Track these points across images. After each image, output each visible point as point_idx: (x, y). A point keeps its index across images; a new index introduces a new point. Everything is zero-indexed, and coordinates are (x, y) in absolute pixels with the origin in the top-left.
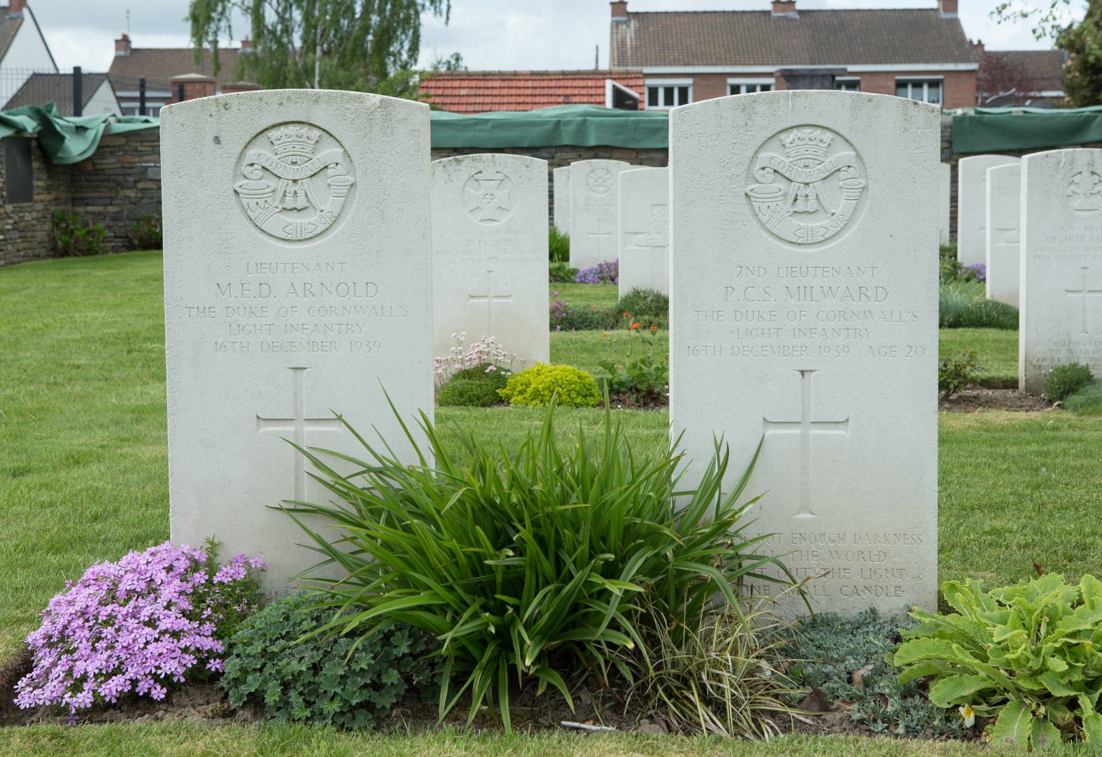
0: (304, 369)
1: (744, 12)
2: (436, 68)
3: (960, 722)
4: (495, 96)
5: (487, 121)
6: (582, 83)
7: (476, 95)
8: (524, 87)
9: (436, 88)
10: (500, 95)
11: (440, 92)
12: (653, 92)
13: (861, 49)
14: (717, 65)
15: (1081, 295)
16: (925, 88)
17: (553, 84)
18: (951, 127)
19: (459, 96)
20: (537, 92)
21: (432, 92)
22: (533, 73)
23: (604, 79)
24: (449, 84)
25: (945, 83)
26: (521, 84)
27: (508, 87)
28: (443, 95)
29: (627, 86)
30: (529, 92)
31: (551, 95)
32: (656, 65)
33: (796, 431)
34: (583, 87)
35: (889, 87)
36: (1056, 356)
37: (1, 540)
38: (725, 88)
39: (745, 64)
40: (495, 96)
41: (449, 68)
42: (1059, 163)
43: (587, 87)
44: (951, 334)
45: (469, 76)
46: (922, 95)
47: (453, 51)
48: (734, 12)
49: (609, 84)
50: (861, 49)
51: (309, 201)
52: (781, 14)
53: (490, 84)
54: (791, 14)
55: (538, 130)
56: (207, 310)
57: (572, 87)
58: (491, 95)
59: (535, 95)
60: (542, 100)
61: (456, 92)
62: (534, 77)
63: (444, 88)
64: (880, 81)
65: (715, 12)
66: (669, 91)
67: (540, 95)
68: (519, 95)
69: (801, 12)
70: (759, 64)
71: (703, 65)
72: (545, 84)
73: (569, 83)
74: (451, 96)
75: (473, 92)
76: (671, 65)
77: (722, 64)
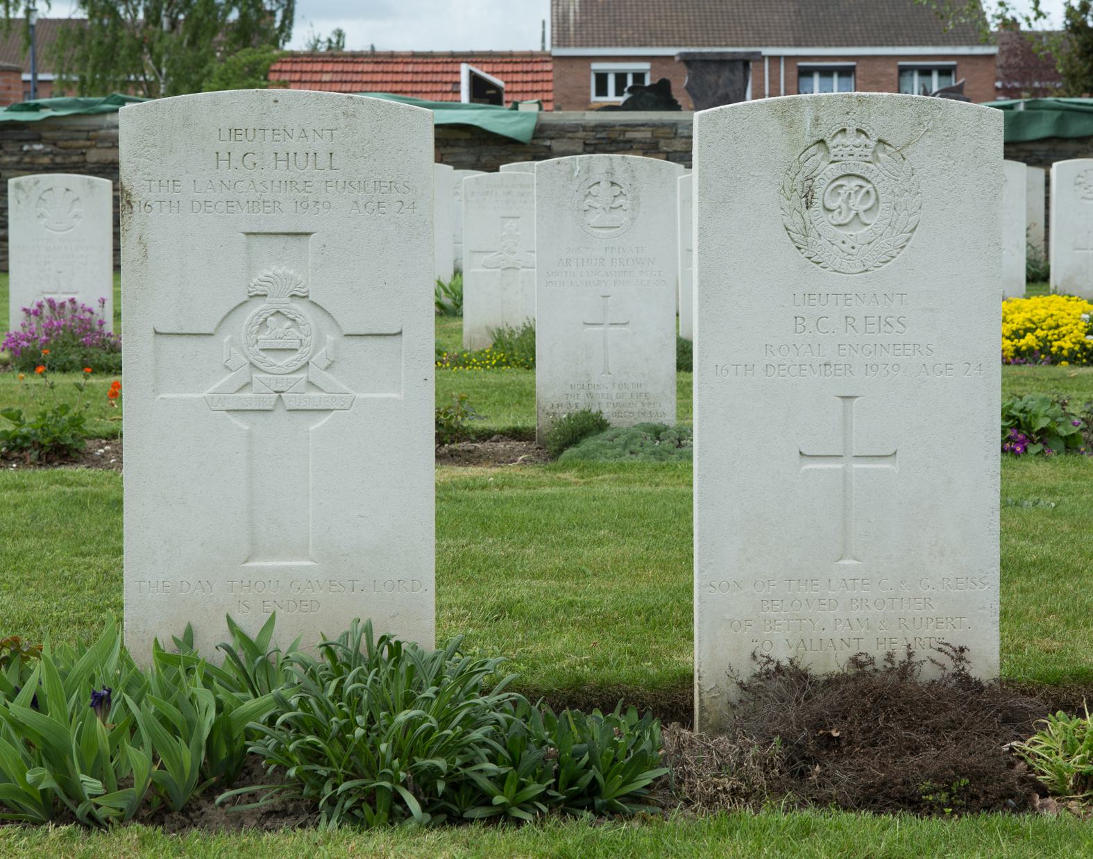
2: (315, 48)
3: (116, 822)
8: (402, 72)
9: (291, 72)
10: (372, 82)
12: (602, 78)
13: (858, 28)
15: (601, 328)
16: (935, 76)
17: (439, 68)
20: (419, 78)
22: (414, 55)
24: (308, 67)
25: (958, 70)
26: (399, 68)
27: (383, 72)
29: (492, 73)
30: (409, 78)
31: (436, 82)
32: (605, 46)
36: (574, 401)
37: (2, 607)
40: (366, 82)
42: (572, 171)
44: (1015, 370)
45: (355, 57)
46: (832, 85)
50: (858, 28)
53: (360, 68)
58: (361, 82)
59: (416, 82)
60: (424, 88)
62: (415, 60)
63: (302, 72)
66: (621, 78)
67: (422, 82)
68: (396, 82)
71: (663, 45)
72: (429, 68)
76: (623, 46)
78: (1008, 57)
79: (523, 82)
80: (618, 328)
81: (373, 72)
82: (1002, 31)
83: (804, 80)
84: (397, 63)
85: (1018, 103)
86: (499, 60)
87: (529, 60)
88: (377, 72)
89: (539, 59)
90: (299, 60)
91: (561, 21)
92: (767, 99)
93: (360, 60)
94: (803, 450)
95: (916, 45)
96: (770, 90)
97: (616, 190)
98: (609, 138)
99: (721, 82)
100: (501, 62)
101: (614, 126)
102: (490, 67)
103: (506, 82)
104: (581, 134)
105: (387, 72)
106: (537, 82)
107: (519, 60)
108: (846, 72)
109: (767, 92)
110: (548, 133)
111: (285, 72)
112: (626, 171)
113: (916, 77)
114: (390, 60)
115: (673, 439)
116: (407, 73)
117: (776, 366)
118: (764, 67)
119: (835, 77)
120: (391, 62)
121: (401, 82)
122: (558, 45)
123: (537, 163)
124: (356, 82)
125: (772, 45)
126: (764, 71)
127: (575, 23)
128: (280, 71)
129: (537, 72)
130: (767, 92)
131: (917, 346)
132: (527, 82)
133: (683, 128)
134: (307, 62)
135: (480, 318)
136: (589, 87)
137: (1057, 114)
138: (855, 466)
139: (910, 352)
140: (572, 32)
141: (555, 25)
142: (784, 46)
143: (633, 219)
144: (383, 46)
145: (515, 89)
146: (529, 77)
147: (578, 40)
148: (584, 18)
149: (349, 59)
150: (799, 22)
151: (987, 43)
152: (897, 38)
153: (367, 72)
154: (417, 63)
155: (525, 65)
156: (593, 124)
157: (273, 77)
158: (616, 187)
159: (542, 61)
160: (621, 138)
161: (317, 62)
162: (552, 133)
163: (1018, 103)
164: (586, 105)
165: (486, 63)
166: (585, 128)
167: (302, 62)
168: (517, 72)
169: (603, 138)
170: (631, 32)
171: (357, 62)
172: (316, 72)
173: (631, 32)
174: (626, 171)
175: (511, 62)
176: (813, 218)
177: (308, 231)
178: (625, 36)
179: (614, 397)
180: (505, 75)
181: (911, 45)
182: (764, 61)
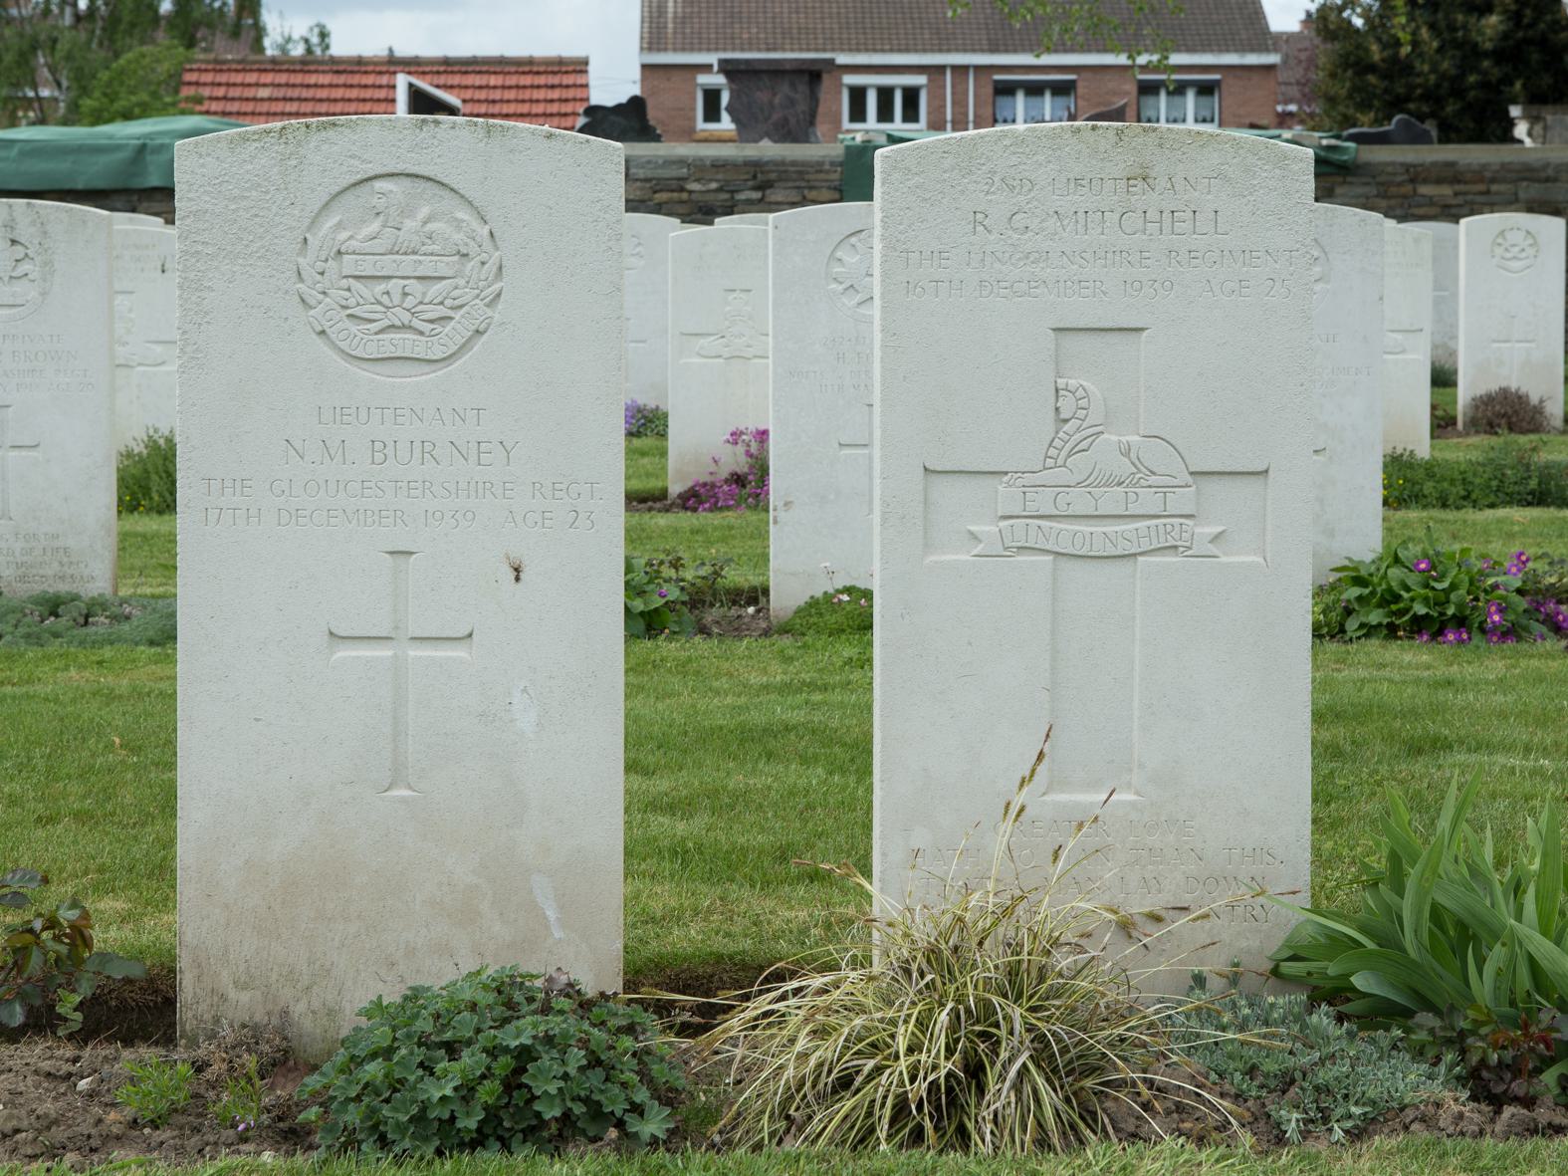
0: (412, 553)
4: (321, 100)
5: (13, 142)
6: (478, 80)
7: (285, 99)
8: (374, 86)
9: (213, 84)
10: (328, 100)
11: (220, 92)
12: (858, 95)
14: (858, 50)
16: (1190, 96)
18: (841, 164)
19: (254, 99)
21: (206, 92)
23: (395, 73)
24: (238, 78)
25: (1224, 86)
26: (369, 80)
28: (225, 98)
33: (384, 652)
34: (480, 87)
38: (840, 93)
39: (875, 51)
40: (321, 100)
41: (309, 51)
43: (487, 87)
47: (312, 22)
49: (402, 81)
53: (312, 79)
55: (104, 160)
56: (238, 484)
58: (313, 99)
61: (249, 93)
63: (228, 85)
66: (885, 95)
70: (900, 51)
74: (241, 99)
75: (280, 93)
78: (1307, 69)
79: (546, 101)
80: (24, 453)
81: (331, 86)
82: (1306, 32)
83: (1003, 101)
84: (366, 72)
86: (513, 69)
87: (556, 69)
88: (337, 86)
89: (570, 68)
90: (225, 67)
91: (655, 15)
92: (972, 132)
93: (312, 68)
94: (334, 631)
97: (19, 251)
99: (777, 100)
100: (517, 72)
103: (464, 101)
105: (352, 86)
106: (566, 100)
107: (542, 69)
108: (1062, 89)
111: (205, 84)
112: (33, 223)
113: (1020, 97)
114: (356, 68)
115: (75, 614)
116: (380, 87)
117: (293, 512)
118: (945, 81)
119: (1048, 96)
120: (358, 72)
121: (371, 100)
122: (650, 49)
123: (771, 216)
124: (306, 100)
125: (957, 50)
126: (944, 87)
127: (675, 17)
128: (197, 84)
129: (567, 86)
130: (1047, 117)
132: (552, 101)
133: (637, 167)
134: (237, 71)
135: (695, 446)
136: (693, 109)
138: (412, 653)
140: (670, 31)
141: (647, 19)
143: (44, 294)
145: (534, 111)
146: (556, 94)
147: (679, 41)
148: (688, 10)
149: (298, 67)
151: (1262, 48)
153: (322, 86)
155: (550, 77)
157: (186, 92)
158: (19, 247)
159: (574, 71)
161: (251, 70)
164: (689, 134)
165: (495, 73)
167: (229, 70)
168: (539, 87)
170: (755, 30)
171: (309, 72)
172: (249, 85)
173: (755, 30)
174: (33, 223)
175: (530, 72)
177: (1140, 325)
178: (745, 36)
179: (17, 554)
180: (463, 91)
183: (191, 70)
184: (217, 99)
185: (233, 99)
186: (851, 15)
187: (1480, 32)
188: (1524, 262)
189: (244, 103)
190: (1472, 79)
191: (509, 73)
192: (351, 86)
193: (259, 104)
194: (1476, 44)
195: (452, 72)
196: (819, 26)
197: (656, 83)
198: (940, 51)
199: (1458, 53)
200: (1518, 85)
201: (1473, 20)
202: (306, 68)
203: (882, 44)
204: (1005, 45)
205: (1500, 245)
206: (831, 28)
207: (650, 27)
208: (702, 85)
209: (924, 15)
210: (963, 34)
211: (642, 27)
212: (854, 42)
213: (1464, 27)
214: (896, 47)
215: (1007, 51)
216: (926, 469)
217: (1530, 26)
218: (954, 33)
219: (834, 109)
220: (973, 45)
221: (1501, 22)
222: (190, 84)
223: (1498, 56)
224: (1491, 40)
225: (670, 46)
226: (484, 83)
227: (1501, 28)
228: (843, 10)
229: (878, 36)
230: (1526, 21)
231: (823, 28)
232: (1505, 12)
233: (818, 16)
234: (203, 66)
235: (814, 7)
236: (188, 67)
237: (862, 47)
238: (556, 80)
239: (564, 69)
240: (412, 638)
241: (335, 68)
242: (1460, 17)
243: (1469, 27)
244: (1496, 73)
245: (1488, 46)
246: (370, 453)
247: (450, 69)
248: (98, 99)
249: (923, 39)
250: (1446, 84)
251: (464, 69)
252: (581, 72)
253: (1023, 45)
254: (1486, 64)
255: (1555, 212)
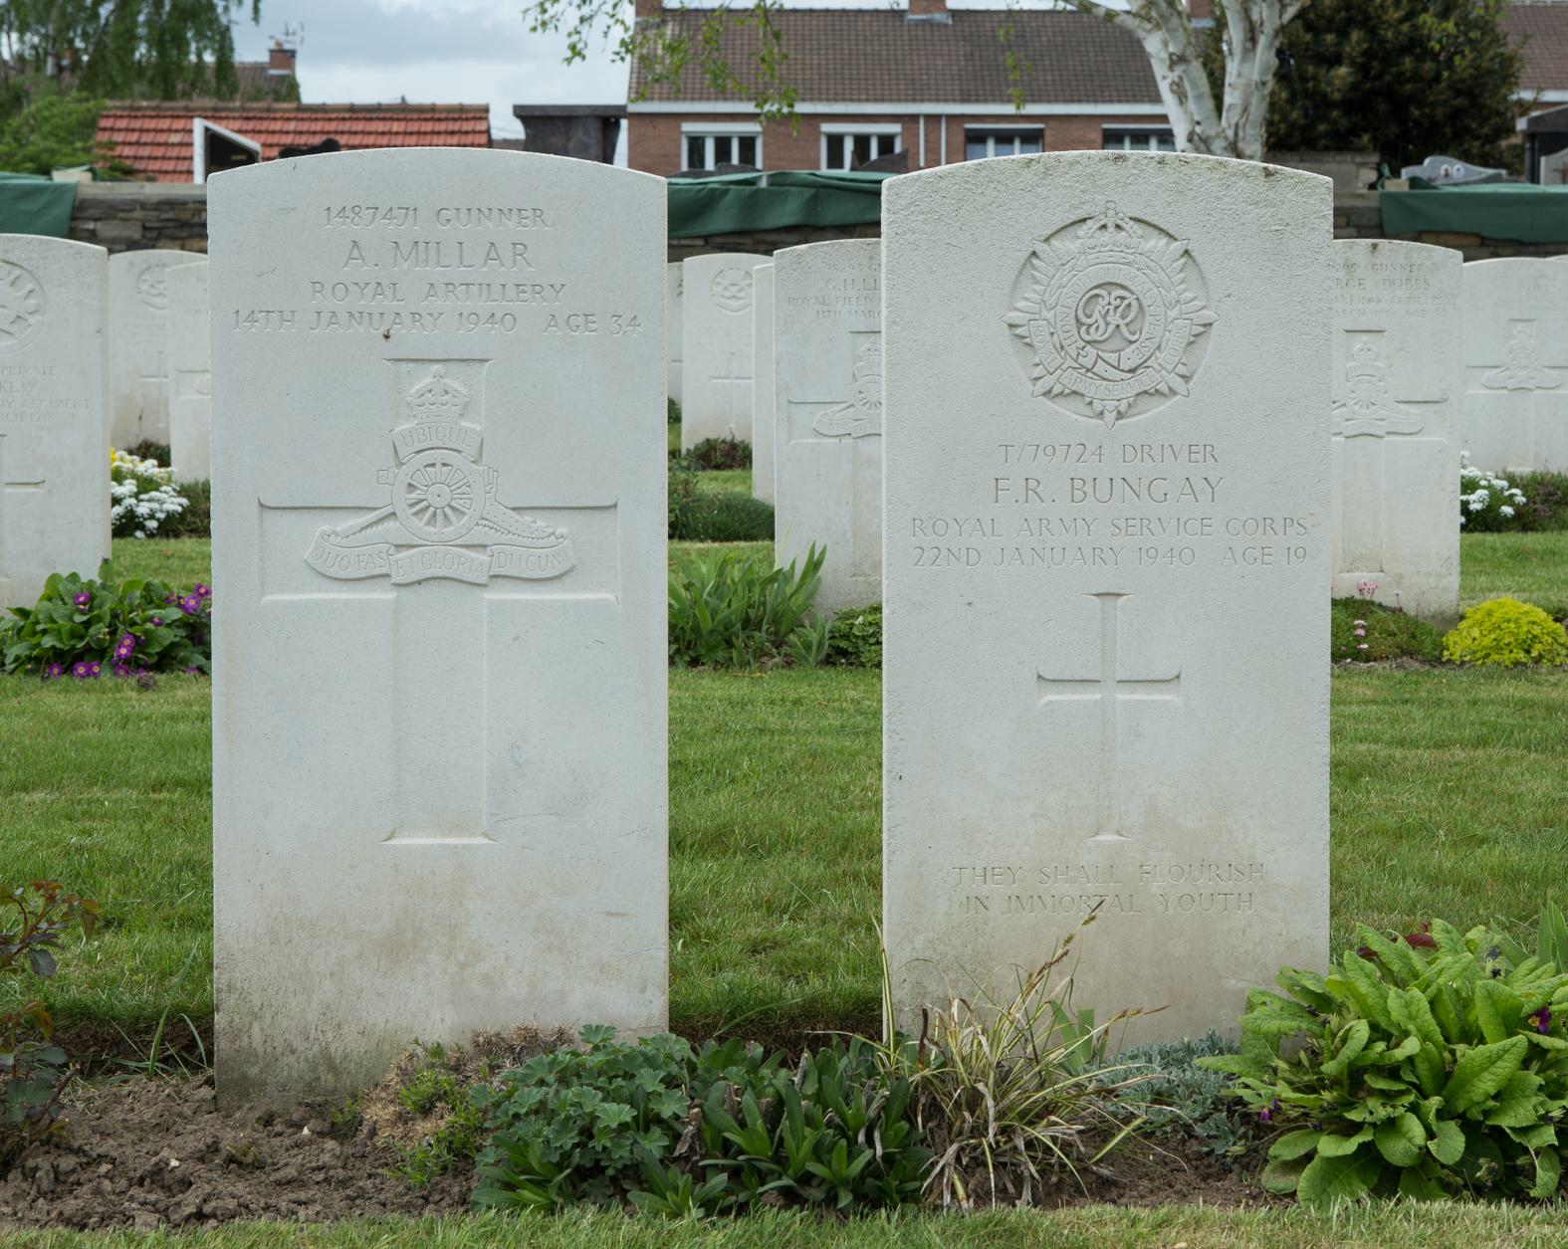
1: (860, 12)
9: (127, 130)
11: (133, 137)
12: (835, 142)
14: (836, 100)
19: (166, 144)
21: (119, 137)
23: (192, 117)
24: (152, 124)
28: (137, 143)
29: (240, 132)
32: (701, 99)
33: (1091, 696)
35: (1093, 141)
38: (818, 140)
43: (390, 133)
48: (844, 12)
50: (1049, 78)
51: (1096, 361)
52: (923, 17)
54: (938, 17)
57: (363, 133)
61: (161, 138)
62: (300, 115)
63: (142, 131)
64: (1077, 131)
65: (811, 11)
66: (862, 142)
69: (954, 13)
73: (360, 126)
74: (153, 144)
77: (812, 100)
84: (274, 119)
85: (760, 177)
86: (415, 116)
87: (456, 116)
89: (470, 115)
90: (139, 114)
93: (223, 114)
95: (1128, 101)
96: (926, 160)
98: (177, 220)
100: (419, 119)
101: (185, 203)
102: (237, 124)
103: (264, 145)
104: (138, 214)
107: (443, 116)
109: (922, 164)
110: (91, 211)
111: (119, 130)
114: (265, 115)
116: (287, 132)
125: (930, 100)
126: (918, 135)
128: (112, 129)
129: (467, 133)
130: (922, 164)
131: (1268, 521)
134: (151, 117)
136: (679, 156)
137: (809, 192)
139: (1136, 530)
142: (946, 101)
144: (416, 98)
150: (970, 68)
152: (1102, 91)
154: (302, 119)
155: (451, 123)
156: (155, 199)
159: (474, 118)
160: (196, 219)
161: (165, 117)
162: (97, 212)
163: (760, 177)
165: (398, 120)
166: (143, 205)
167: (144, 117)
169: (169, 220)
172: (162, 131)
176: (1064, 343)
181: (1120, 101)
182: (918, 123)
183: (107, 117)
184: (130, 144)
185: (145, 144)
186: (831, 67)
187: (1329, 83)
188: (741, 302)
189: (156, 148)
190: (1322, 128)
191: (412, 120)
192: (356, 133)
193: (170, 148)
194: (1325, 95)
195: (357, 119)
196: (800, 77)
197: (642, 130)
198: (914, 101)
199: (1308, 103)
200: (1366, 138)
201: (1323, 72)
202: (218, 115)
203: (859, 94)
204: (977, 95)
205: (719, 283)
206: (811, 79)
207: (638, 78)
208: (686, 133)
209: (900, 67)
210: (937, 84)
211: (631, 78)
212: (832, 92)
213: (1315, 78)
214: (871, 97)
215: (977, 101)
216: (261, 505)
217: (1378, 77)
218: (928, 84)
219: (812, 155)
220: (946, 95)
221: (1349, 74)
222: (105, 129)
223: (1347, 105)
224: (1339, 90)
225: (656, 96)
226: (386, 129)
227: (1350, 79)
228: (823, 62)
229: (855, 87)
230: (1373, 72)
231: (804, 79)
232: (1353, 64)
233: (799, 67)
234: (119, 113)
235: (796, 59)
236: (104, 113)
237: (840, 97)
238: (455, 126)
239: (464, 116)
240: (1119, 682)
241: (245, 115)
242: (1311, 68)
243: (1319, 77)
244: (1344, 123)
245: (1337, 96)
246: (994, 491)
247: (355, 116)
248: (8, 144)
249: (898, 89)
250: (1296, 133)
251: (368, 116)
252: (481, 119)
253: (993, 95)
254: (1335, 114)
255: (1563, 253)
